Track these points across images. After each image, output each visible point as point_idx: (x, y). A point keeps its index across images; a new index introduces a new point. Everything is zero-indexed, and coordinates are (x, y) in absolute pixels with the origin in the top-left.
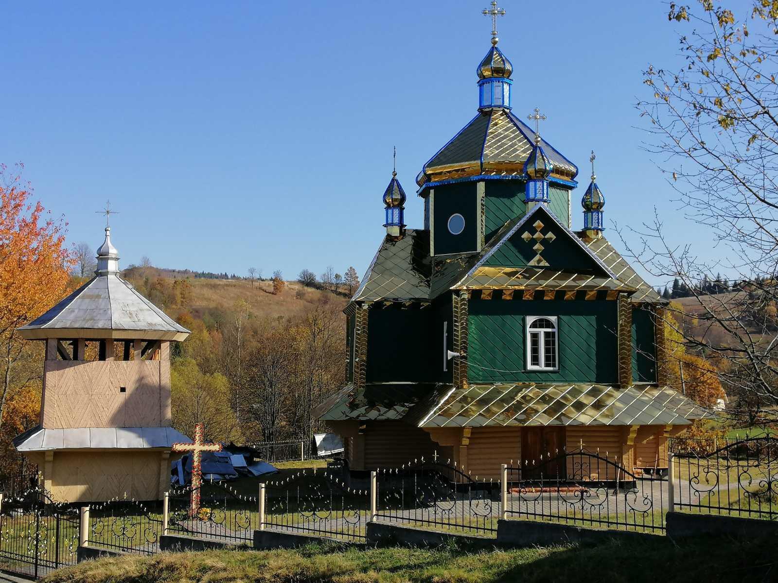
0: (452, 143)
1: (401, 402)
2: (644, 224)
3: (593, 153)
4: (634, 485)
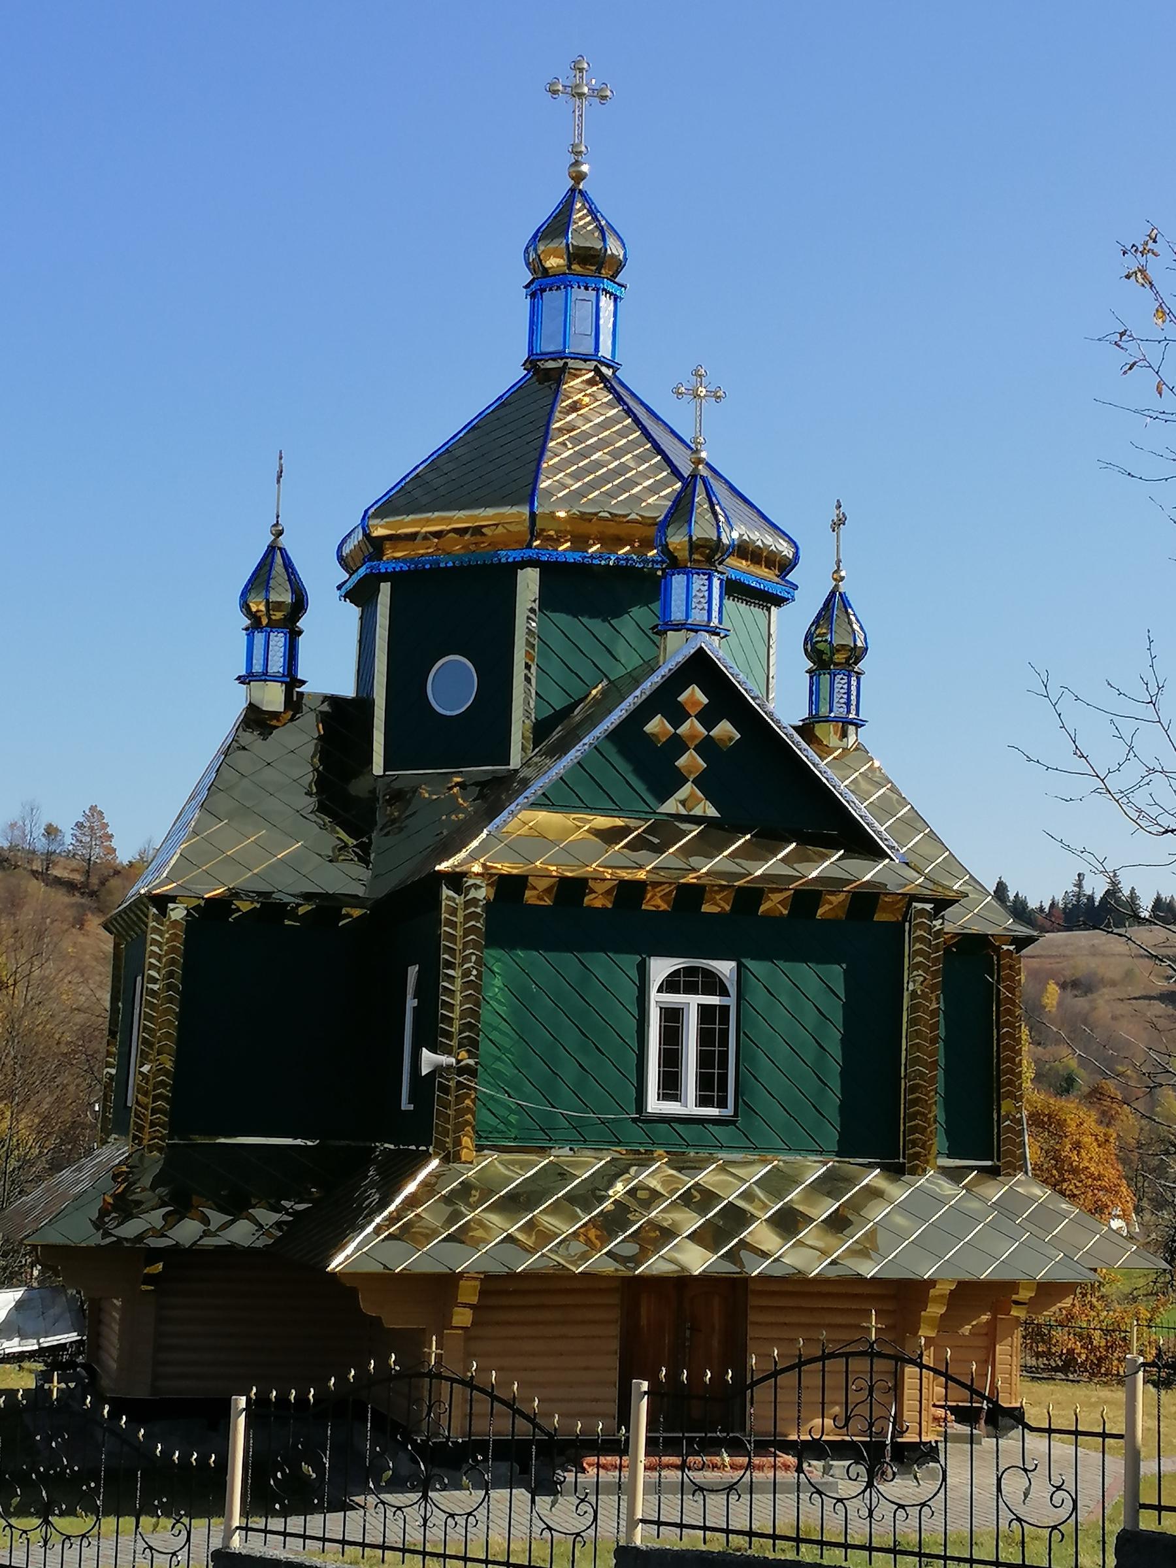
2: (1109, 684)
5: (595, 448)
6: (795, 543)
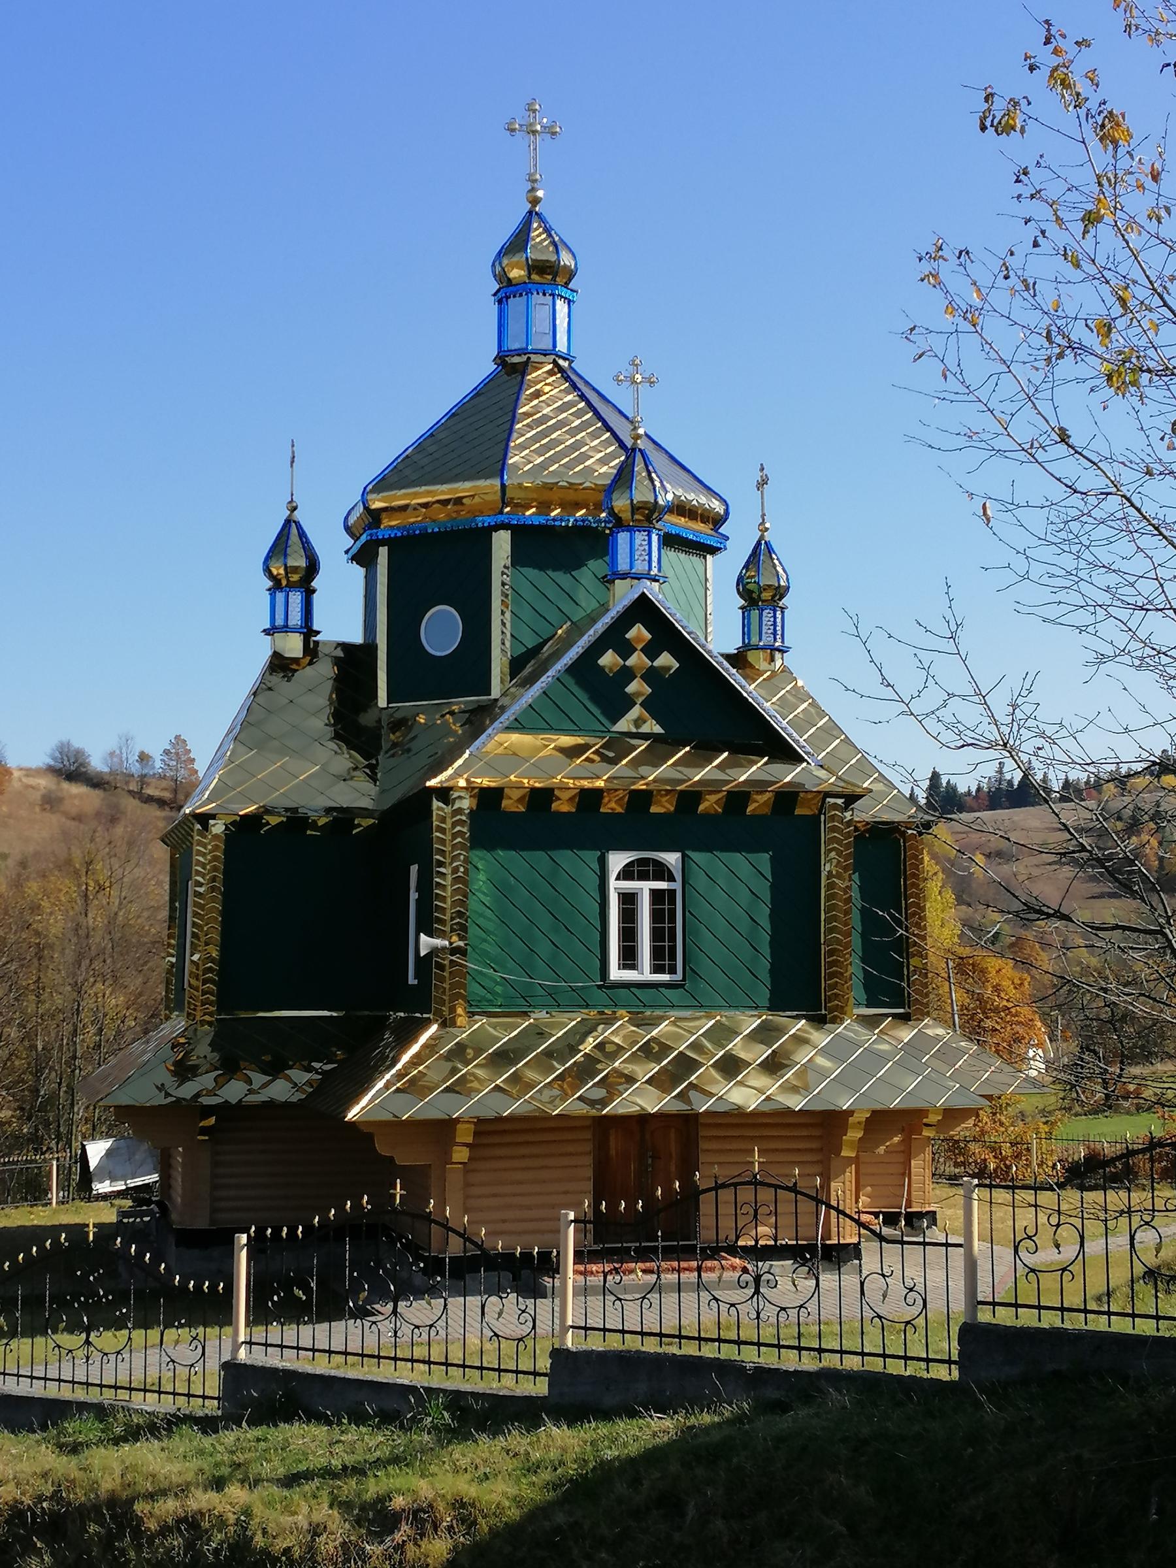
0: (431, 435)
1: (305, 1062)
3: (762, 469)
4: (855, 1251)
5: (555, 428)
6: (725, 502)
